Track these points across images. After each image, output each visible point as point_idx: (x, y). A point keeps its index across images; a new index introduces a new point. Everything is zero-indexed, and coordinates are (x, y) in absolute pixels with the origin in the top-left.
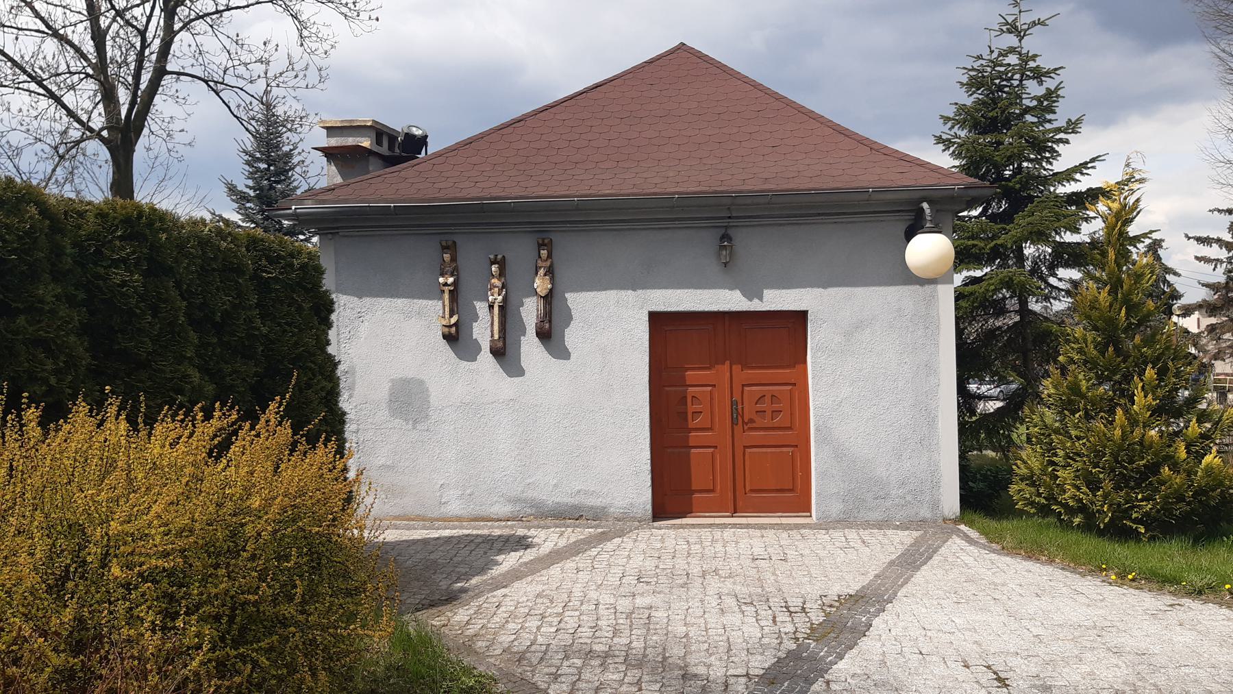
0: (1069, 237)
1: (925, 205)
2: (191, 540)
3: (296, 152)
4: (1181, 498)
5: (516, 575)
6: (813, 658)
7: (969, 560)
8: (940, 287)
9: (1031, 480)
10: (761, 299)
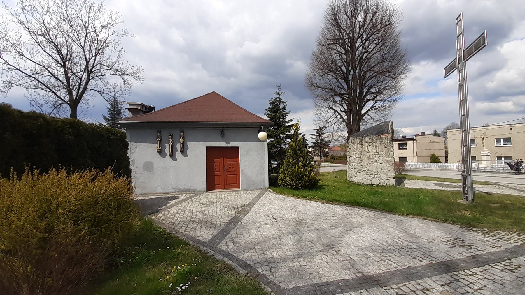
0: (288, 133)
1: (262, 126)
2: (83, 202)
3: (122, 109)
4: (307, 182)
5: (174, 205)
6: (239, 218)
7: (270, 196)
8: (265, 142)
9: (282, 179)
10: (230, 144)
